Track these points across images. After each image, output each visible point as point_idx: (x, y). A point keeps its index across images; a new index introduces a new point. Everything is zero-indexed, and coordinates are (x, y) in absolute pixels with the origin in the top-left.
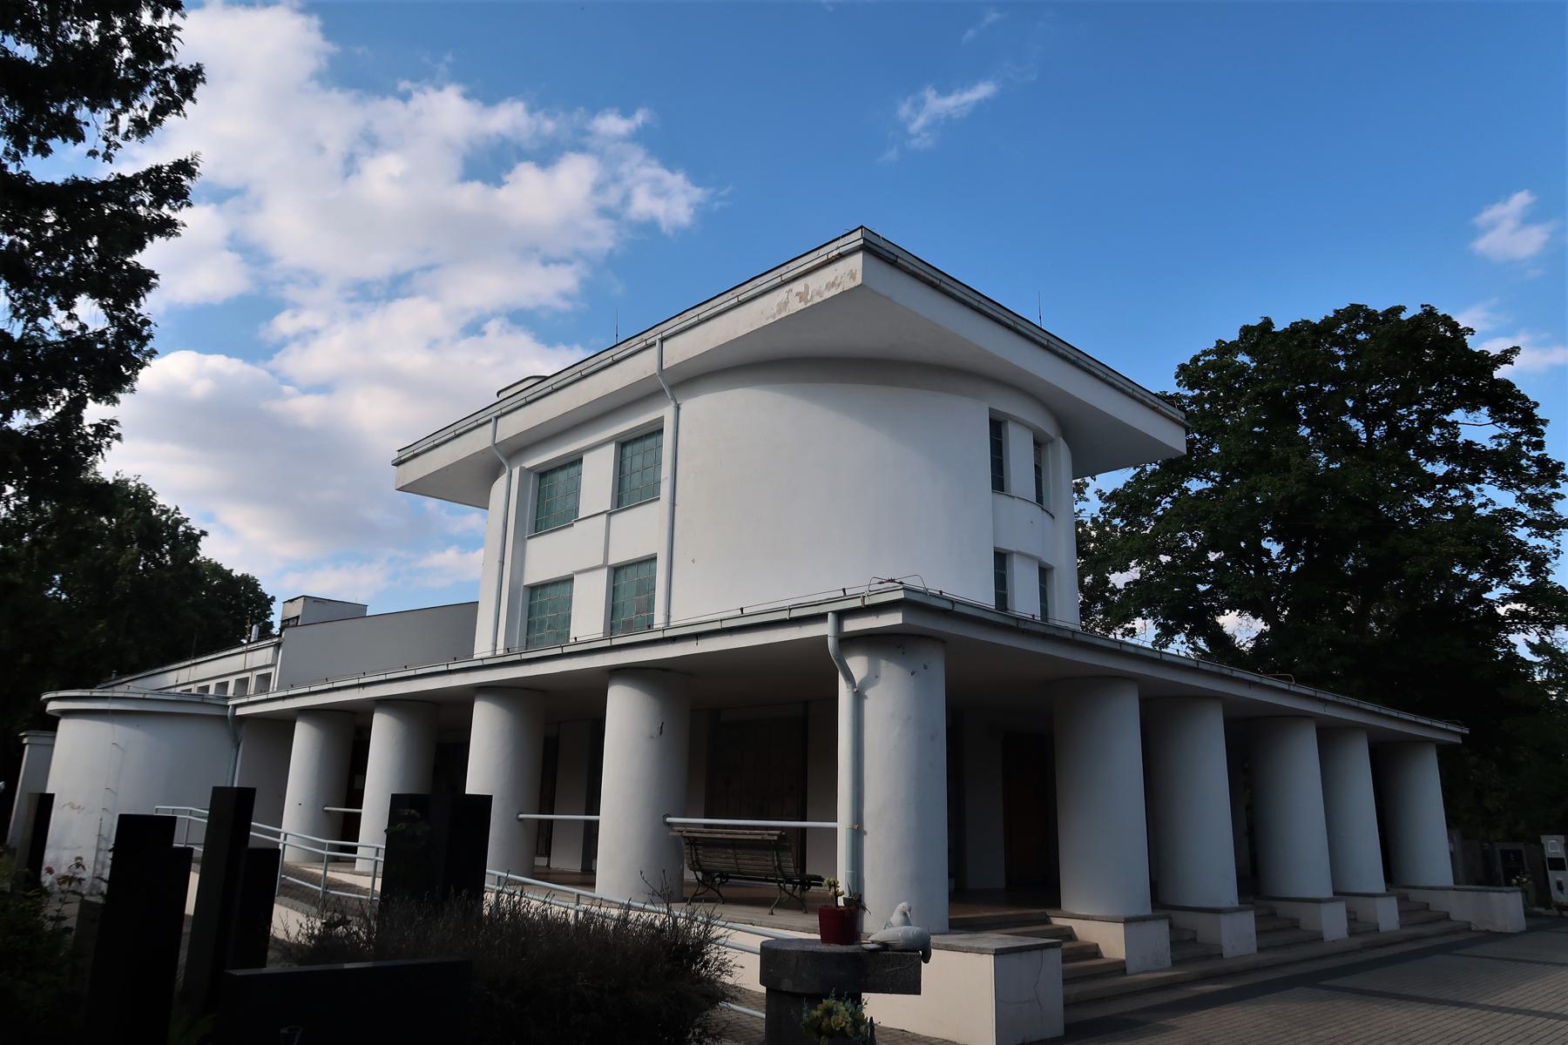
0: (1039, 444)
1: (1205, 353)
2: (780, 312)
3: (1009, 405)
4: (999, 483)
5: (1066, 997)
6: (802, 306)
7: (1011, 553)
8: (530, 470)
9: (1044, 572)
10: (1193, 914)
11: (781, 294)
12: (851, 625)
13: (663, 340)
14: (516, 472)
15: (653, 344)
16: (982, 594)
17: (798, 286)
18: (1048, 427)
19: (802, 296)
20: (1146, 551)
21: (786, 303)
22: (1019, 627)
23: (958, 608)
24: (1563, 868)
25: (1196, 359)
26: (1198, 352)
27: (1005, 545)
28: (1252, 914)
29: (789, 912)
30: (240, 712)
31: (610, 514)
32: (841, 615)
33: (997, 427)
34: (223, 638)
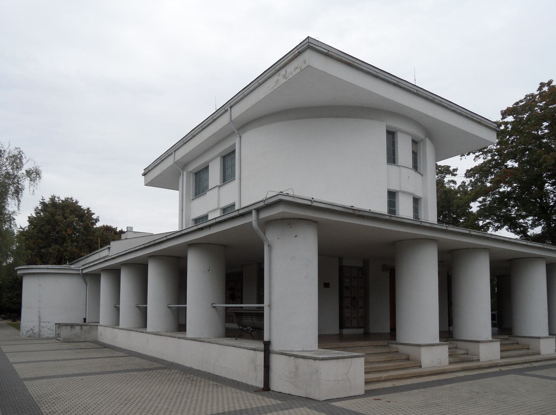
0: (415, 142)
1: (521, 101)
2: (275, 85)
3: (395, 124)
4: (392, 158)
5: (365, 380)
6: (284, 81)
7: (398, 191)
8: (190, 172)
9: (416, 201)
10: (467, 343)
11: (276, 78)
12: (264, 215)
13: (231, 107)
14: (185, 173)
15: (227, 110)
16: (382, 208)
17: (283, 72)
18: (420, 134)
19: (284, 76)
20: (486, 192)
21: (278, 80)
22: (402, 223)
23: (315, 204)
24: (325, 283)
25: (517, 103)
26: (518, 100)
27: (394, 188)
28: (499, 343)
29: (248, 341)
30: (84, 272)
31: (220, 187)
32: (258, 210)
33: (391, 135)
34: (92, 248)
